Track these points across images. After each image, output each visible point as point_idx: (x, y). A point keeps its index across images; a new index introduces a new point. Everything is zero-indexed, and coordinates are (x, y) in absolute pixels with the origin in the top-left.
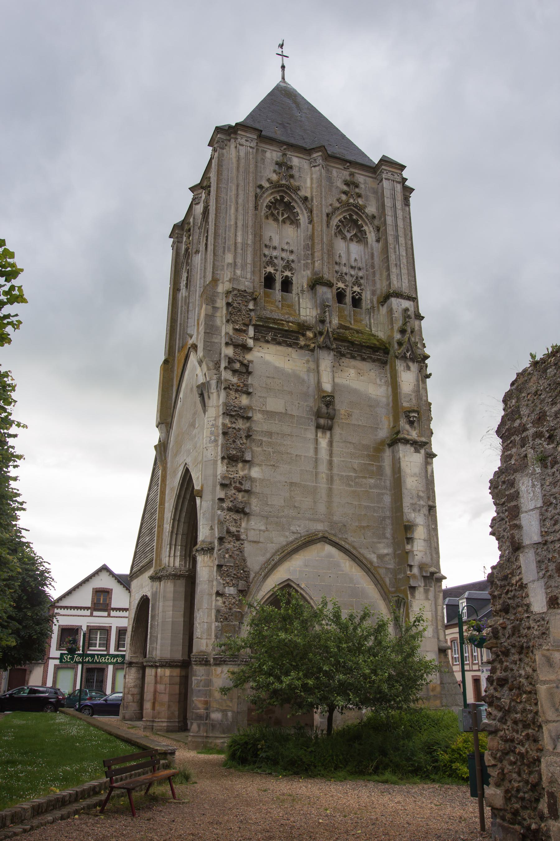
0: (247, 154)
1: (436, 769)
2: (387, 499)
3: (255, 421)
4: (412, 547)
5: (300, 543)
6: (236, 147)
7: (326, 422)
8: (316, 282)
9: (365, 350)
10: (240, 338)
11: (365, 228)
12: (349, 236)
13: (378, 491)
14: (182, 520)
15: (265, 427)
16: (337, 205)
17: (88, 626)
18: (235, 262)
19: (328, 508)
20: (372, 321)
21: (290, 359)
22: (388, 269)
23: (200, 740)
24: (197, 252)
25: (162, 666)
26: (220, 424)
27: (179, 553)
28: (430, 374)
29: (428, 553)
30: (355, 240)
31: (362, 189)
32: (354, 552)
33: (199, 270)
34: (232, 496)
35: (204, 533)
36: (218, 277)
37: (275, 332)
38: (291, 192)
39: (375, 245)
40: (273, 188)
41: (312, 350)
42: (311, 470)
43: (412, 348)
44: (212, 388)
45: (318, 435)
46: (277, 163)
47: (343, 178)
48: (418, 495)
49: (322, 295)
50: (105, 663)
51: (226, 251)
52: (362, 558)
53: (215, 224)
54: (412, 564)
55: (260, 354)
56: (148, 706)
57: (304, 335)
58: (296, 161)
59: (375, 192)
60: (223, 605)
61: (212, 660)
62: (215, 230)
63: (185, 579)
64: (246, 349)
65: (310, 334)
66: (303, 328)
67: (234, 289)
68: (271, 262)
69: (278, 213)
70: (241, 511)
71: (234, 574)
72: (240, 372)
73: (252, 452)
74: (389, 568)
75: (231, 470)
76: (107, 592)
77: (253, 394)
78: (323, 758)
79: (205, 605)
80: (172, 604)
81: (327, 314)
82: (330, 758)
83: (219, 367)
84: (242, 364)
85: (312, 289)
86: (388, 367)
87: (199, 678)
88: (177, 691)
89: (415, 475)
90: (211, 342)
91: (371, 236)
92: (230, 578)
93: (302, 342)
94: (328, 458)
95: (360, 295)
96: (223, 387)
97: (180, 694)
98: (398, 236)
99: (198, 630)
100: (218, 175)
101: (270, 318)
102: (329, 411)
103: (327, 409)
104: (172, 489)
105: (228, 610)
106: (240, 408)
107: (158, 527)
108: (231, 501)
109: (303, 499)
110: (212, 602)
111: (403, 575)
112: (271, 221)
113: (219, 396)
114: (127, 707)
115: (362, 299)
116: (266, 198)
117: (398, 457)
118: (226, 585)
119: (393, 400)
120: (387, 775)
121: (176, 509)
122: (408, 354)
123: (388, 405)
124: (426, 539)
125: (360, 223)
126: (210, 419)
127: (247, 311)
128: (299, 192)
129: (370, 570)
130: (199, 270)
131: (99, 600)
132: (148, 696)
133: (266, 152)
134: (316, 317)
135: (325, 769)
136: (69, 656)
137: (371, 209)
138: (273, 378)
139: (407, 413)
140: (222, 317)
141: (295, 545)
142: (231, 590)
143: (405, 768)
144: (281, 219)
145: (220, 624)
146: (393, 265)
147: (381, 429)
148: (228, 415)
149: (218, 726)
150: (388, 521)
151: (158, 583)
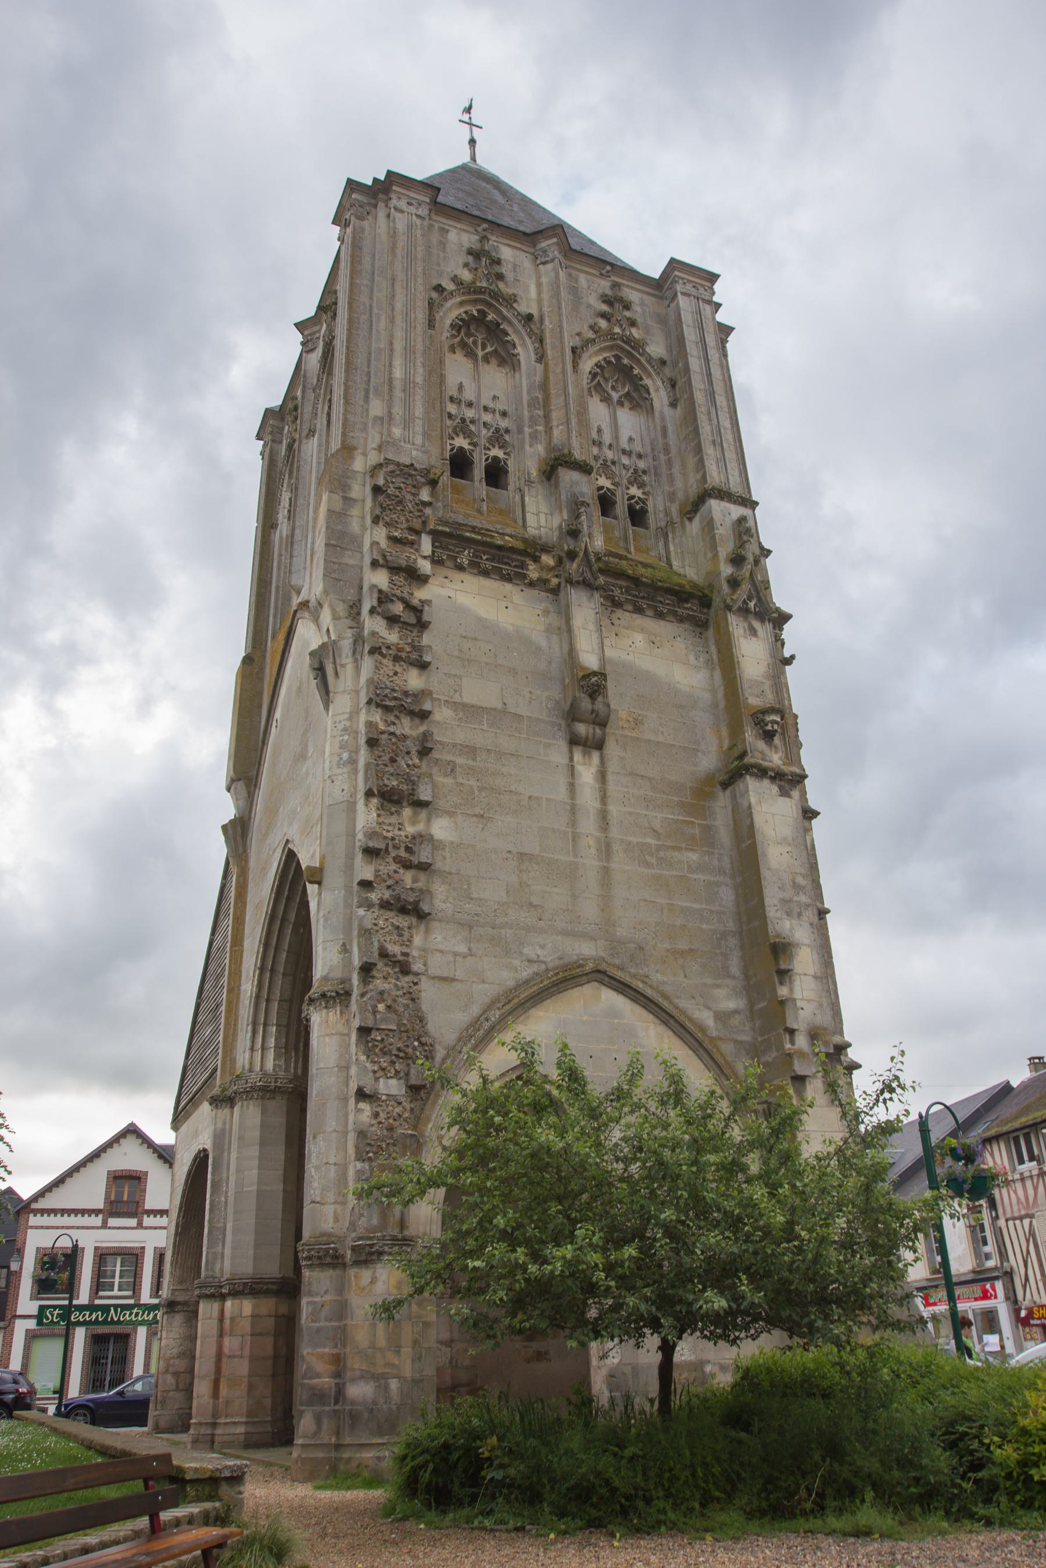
0: (410, 227)
1: (988, 1491)
2: (727, 895)
3: (438, 722)
4: (791, 990)
5: (545, 983)
6: (388, 216)
7: (591, 731)
8: (555, 465)
9: (662, 596)
10: (402, 556)
11: (647, 381)
12: (615, 396)
13: (708, 877)
14: (281, 969)
15: (461, 736)
16: (591, 335)
17: (96, 1248)
18: (390, 413)
19: (603, 910)
20: (672, 548)
21: (510, 605)
22: (699, 450)
23: (320, 1454)
24: (312, 432)
25: (235, 1294)
26: (362, 728)
27: (273, 1040)
28: (793, 657)
29: (825, 1004)
30: (627, 403)
31: (637, 312)
32: (665, 1004)
33: (314, 465)
34: (389, 876)
35: (326, 960)
36: (354, 443)
37: (476, 551)
38: (501, 304)
39: (668, 411)
40: (463, 294)
41: (555, 591)
42: (563, 828)
43: (758, 593)
44: (344, 655)
45: (576, 758)
46: (470, 252)
47: (600, 291)
48: (794, 883)
49: (571, 487)
50: (131, 1322)
51: (371, 396)
52: (682, 1018)
53: (348, 348)
54: (795, 1027)
55: (445, 592)
56: (202, 1388)
57: (536, 559)
58: (507, 253)
59: (662, 321)
60: (374, 1122)
61: (349, 1252)
62: (347, 358)
63: (286, 1097)
64: (418, 579)
65: (548, 560)
66: (533, 549)
67: (388, 461)
68: (463, 427)
69: (475, 343)
70: (412, 910)
71: (399, 1049)
72: (404, 623)
73: (434, 785)
74: (741, 1042)
75: (386, 821)
76: (136, 1179)
77: (432, 667)
78: (667, 1475)
79: (331, 1124)
80: (257, 1154)
81: (583, 518)
82: (687, 1473)
83: (359, 614)
84: (408, 606)
85: (549, 479)
86: (710, 633)
87: (318, 1299)
88: (269, 1351)
89: (784, 841)
90: (340, 564)
91: (660, 397)
92: (387, 1058)
93: (533, 572)
94: (598, 805)
95: (644, 503)
96: (366, 650)
97: (276, 1357)
98: (714, 392)
99: (316, 1184)
100: (352, 263)
101: (464, 525)
102: (596, 707)
103: (593, 704)
104: (257, 907)
105: (385, 1132)
106: (406, 693)
107: (228, 991)
108: (389, 887)
109: (548, 889)
110: (346, 1115)
111: (774, 1054)
112: (459, 356)
113: (358, 669)
114: (164, 1402)
115: (647, 511)
116: (450, 309)
117: (745, 805)
118: (380, 1073)
119: (726, 695)
120: (867, 1515)
121: (266, 945)
122: (752, 604)
123: (715, 705)
124: (819, 974)
125: (636, 372)
126: (338, 718)
127: (417, 504)
128: (515, 305)
129: (701, 1044)
130: (314, 465)
131: (119, 1194)
132: (204, 1366)
133: (448, 231)
134: (560, 527)
135: (675, 1506)
136: (57, 1312)
137: (656, 349)
138: (476, 639)
139: (759, 717)
140: (363, 518)
141: (535, 988)
142: (391, 1087)
143: (899, 1489)
144: (480, 353)
145: (366, 1165)
146: (707, 444)
147: (704, 753)
148: (378, 705)
149: (366, 1415)
150: (732, 942)
151: (227, 1111)
